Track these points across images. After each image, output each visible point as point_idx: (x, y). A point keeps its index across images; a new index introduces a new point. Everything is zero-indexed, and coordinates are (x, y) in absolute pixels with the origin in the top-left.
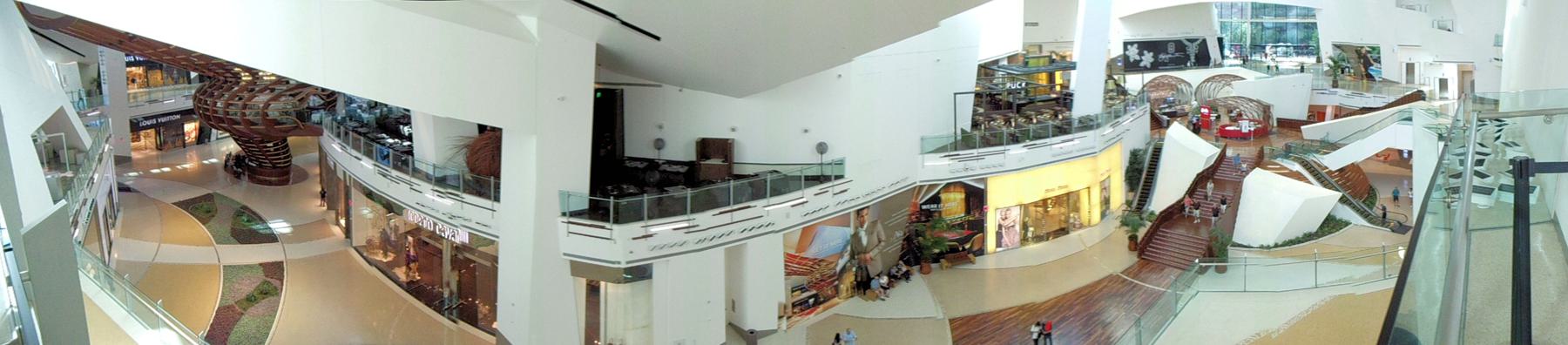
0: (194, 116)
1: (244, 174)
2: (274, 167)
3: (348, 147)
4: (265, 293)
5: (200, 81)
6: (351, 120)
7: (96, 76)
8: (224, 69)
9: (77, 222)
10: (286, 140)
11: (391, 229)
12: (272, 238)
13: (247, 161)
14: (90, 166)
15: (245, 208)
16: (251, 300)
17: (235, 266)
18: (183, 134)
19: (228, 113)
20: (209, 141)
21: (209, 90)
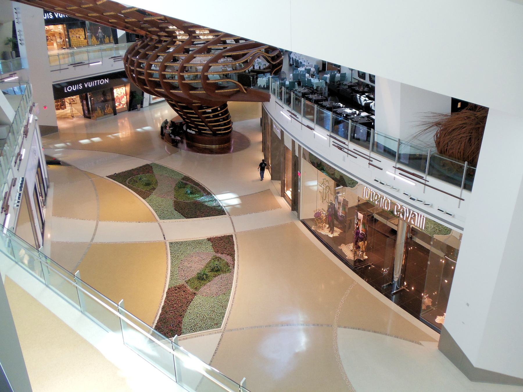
0: (124, 80)
1: (182, 142)
2: (214, 134)
3: (298, 115)
4: (216, 270)
5: (128, 41)
6: (299, 84)
7: (10, 35)
8: (158, 28)
9: (8, 206)
10: (226, 105)
11: (339, 203)
12: (218, 211)
13: (184, 128)
14: (16, 140)
15: (187, 179)
16: (202, 278)
17: (182, 242)
18: (113, 99)
19: (164, 77)
20: (142, 107)
21: (142, 51)
